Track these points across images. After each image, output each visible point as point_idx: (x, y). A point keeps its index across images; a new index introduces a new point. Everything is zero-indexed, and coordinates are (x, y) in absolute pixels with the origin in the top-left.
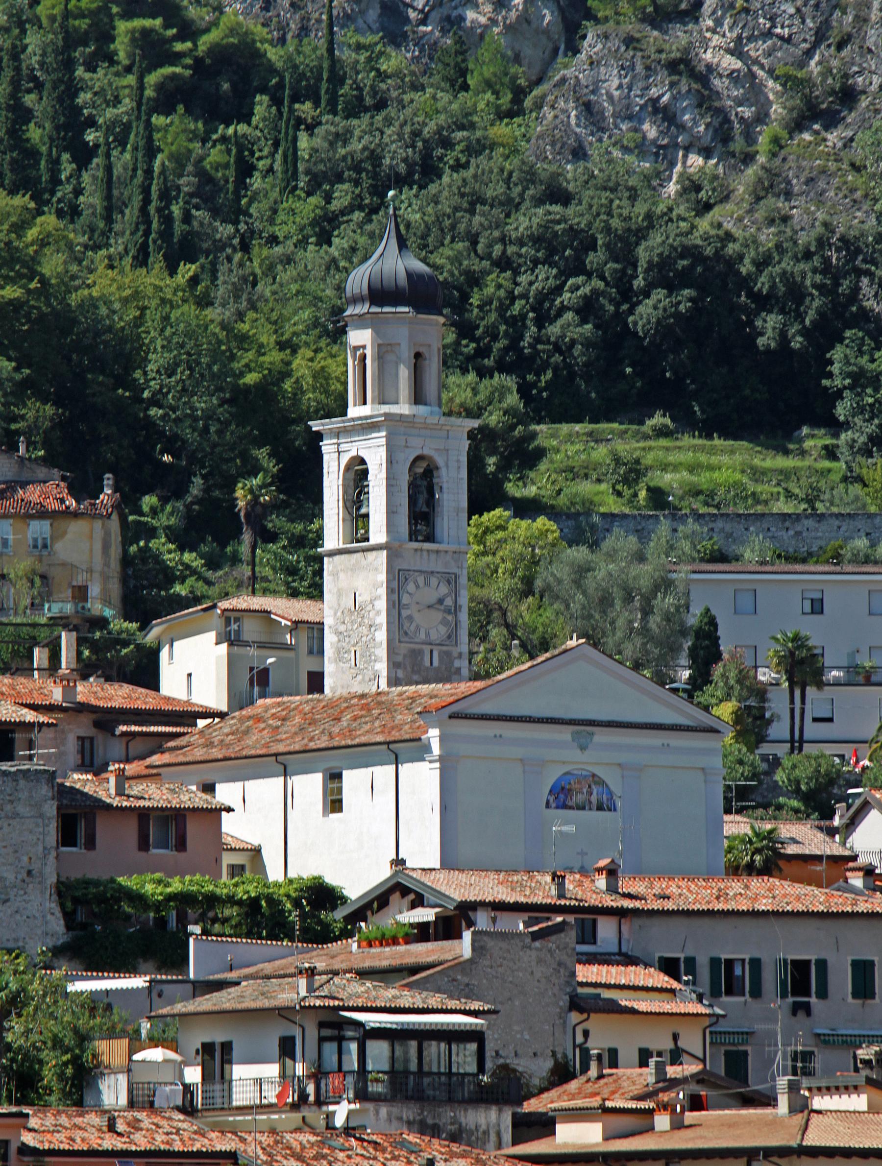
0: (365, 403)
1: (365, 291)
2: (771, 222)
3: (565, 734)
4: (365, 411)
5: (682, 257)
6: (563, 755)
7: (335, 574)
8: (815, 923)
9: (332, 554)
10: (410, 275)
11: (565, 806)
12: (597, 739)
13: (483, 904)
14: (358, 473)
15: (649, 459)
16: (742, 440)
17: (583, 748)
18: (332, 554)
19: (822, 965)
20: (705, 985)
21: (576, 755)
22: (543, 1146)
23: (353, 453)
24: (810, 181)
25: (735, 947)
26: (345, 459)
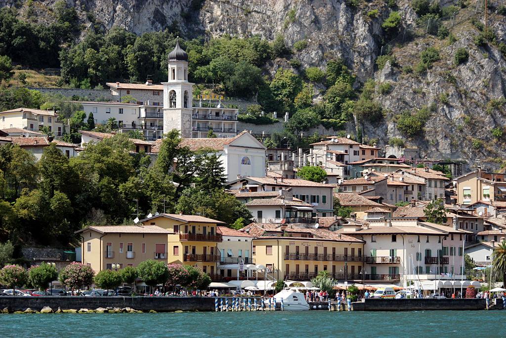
0: (174, 79)
1: (175, 56)
2: (33, 21)
3: (244, 149)
4: (175, 81)
5: (23, 29)
6: (243, 153)
7: (166, 114)
8: (317, 188)
9: (165, 110)
10: (184, 53)
11: (243, 164)
12: (249, 150)
13: (266, 184)
14: (173, 94)
15: (27, 75)
16: (32, 70)
17: (247, 152)
18: (165, 110)
19: (318, 196)
20: (309, 201)
21: (246, 154)
22: (431, 231)
23: (172, 89)
24: (41, 12)
25: (314, 193)
26: (169, 91)
